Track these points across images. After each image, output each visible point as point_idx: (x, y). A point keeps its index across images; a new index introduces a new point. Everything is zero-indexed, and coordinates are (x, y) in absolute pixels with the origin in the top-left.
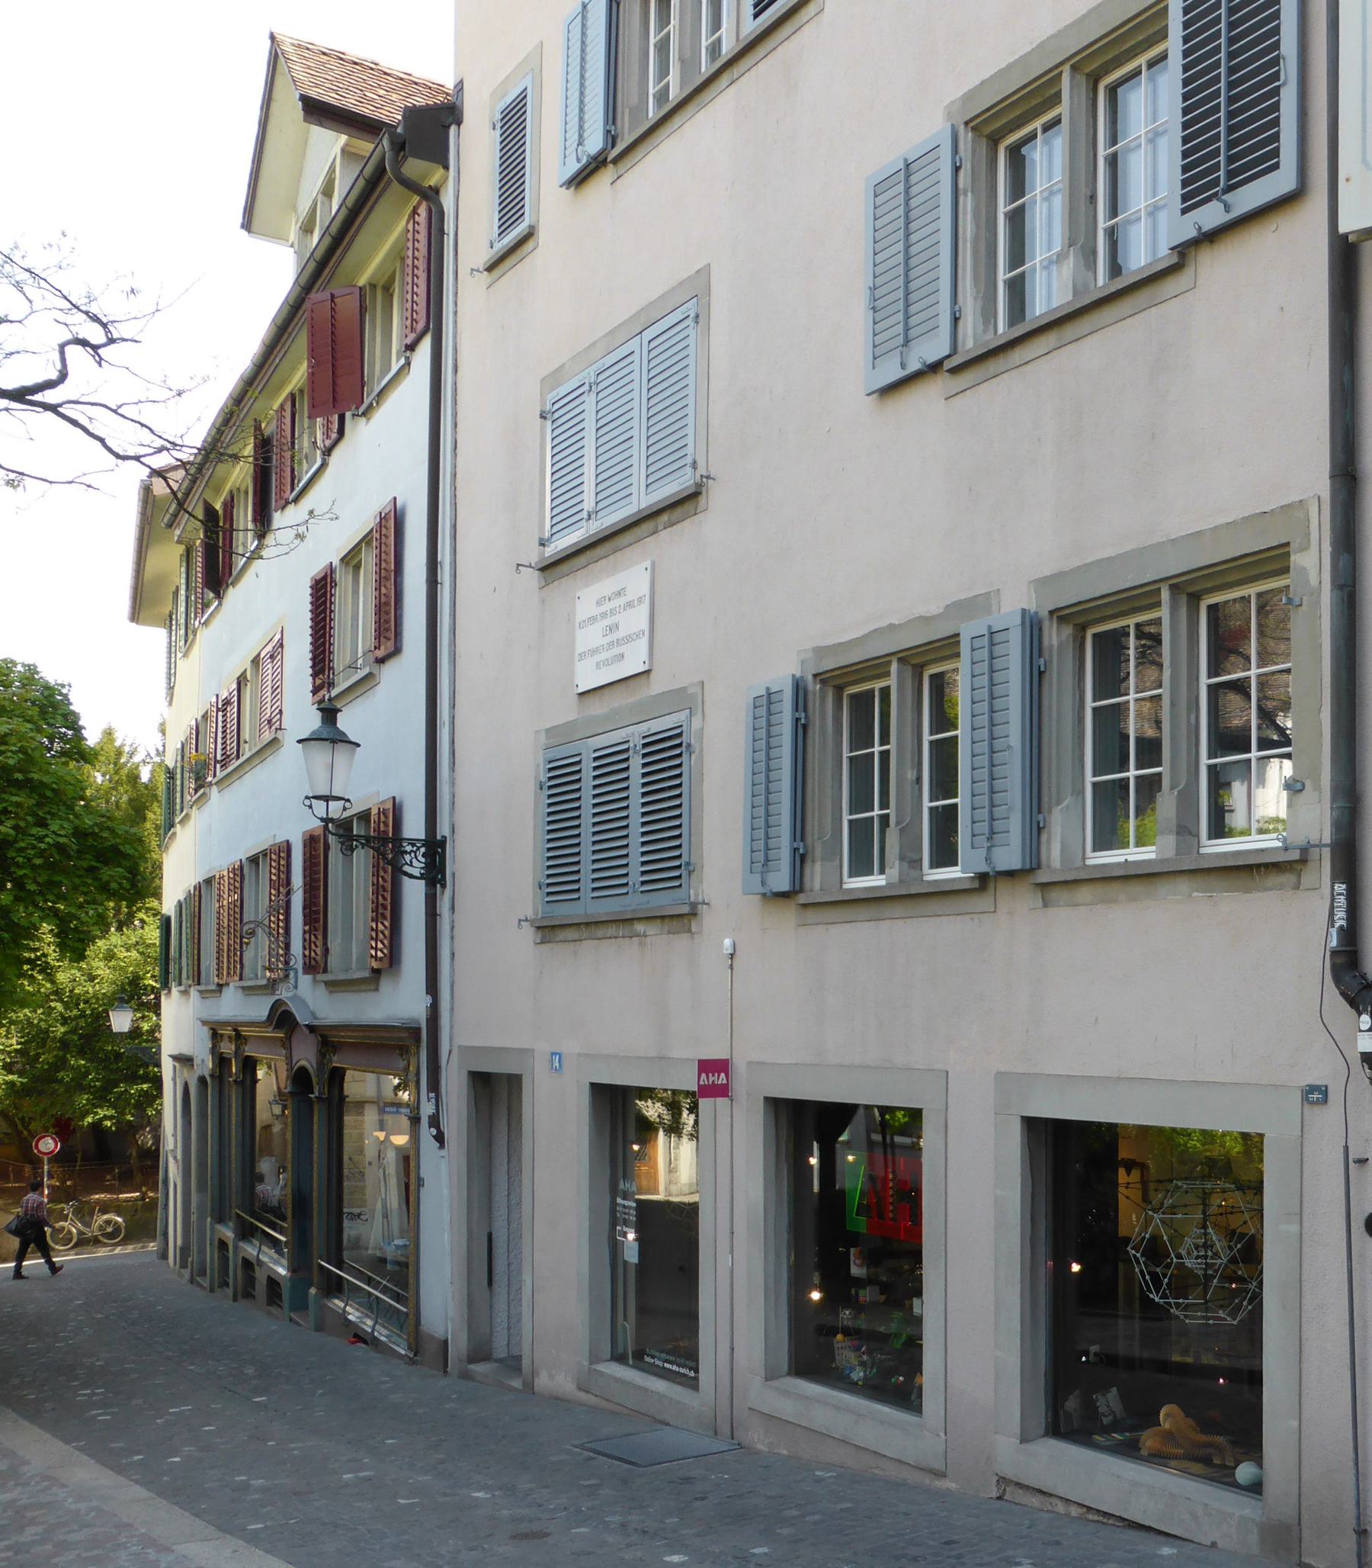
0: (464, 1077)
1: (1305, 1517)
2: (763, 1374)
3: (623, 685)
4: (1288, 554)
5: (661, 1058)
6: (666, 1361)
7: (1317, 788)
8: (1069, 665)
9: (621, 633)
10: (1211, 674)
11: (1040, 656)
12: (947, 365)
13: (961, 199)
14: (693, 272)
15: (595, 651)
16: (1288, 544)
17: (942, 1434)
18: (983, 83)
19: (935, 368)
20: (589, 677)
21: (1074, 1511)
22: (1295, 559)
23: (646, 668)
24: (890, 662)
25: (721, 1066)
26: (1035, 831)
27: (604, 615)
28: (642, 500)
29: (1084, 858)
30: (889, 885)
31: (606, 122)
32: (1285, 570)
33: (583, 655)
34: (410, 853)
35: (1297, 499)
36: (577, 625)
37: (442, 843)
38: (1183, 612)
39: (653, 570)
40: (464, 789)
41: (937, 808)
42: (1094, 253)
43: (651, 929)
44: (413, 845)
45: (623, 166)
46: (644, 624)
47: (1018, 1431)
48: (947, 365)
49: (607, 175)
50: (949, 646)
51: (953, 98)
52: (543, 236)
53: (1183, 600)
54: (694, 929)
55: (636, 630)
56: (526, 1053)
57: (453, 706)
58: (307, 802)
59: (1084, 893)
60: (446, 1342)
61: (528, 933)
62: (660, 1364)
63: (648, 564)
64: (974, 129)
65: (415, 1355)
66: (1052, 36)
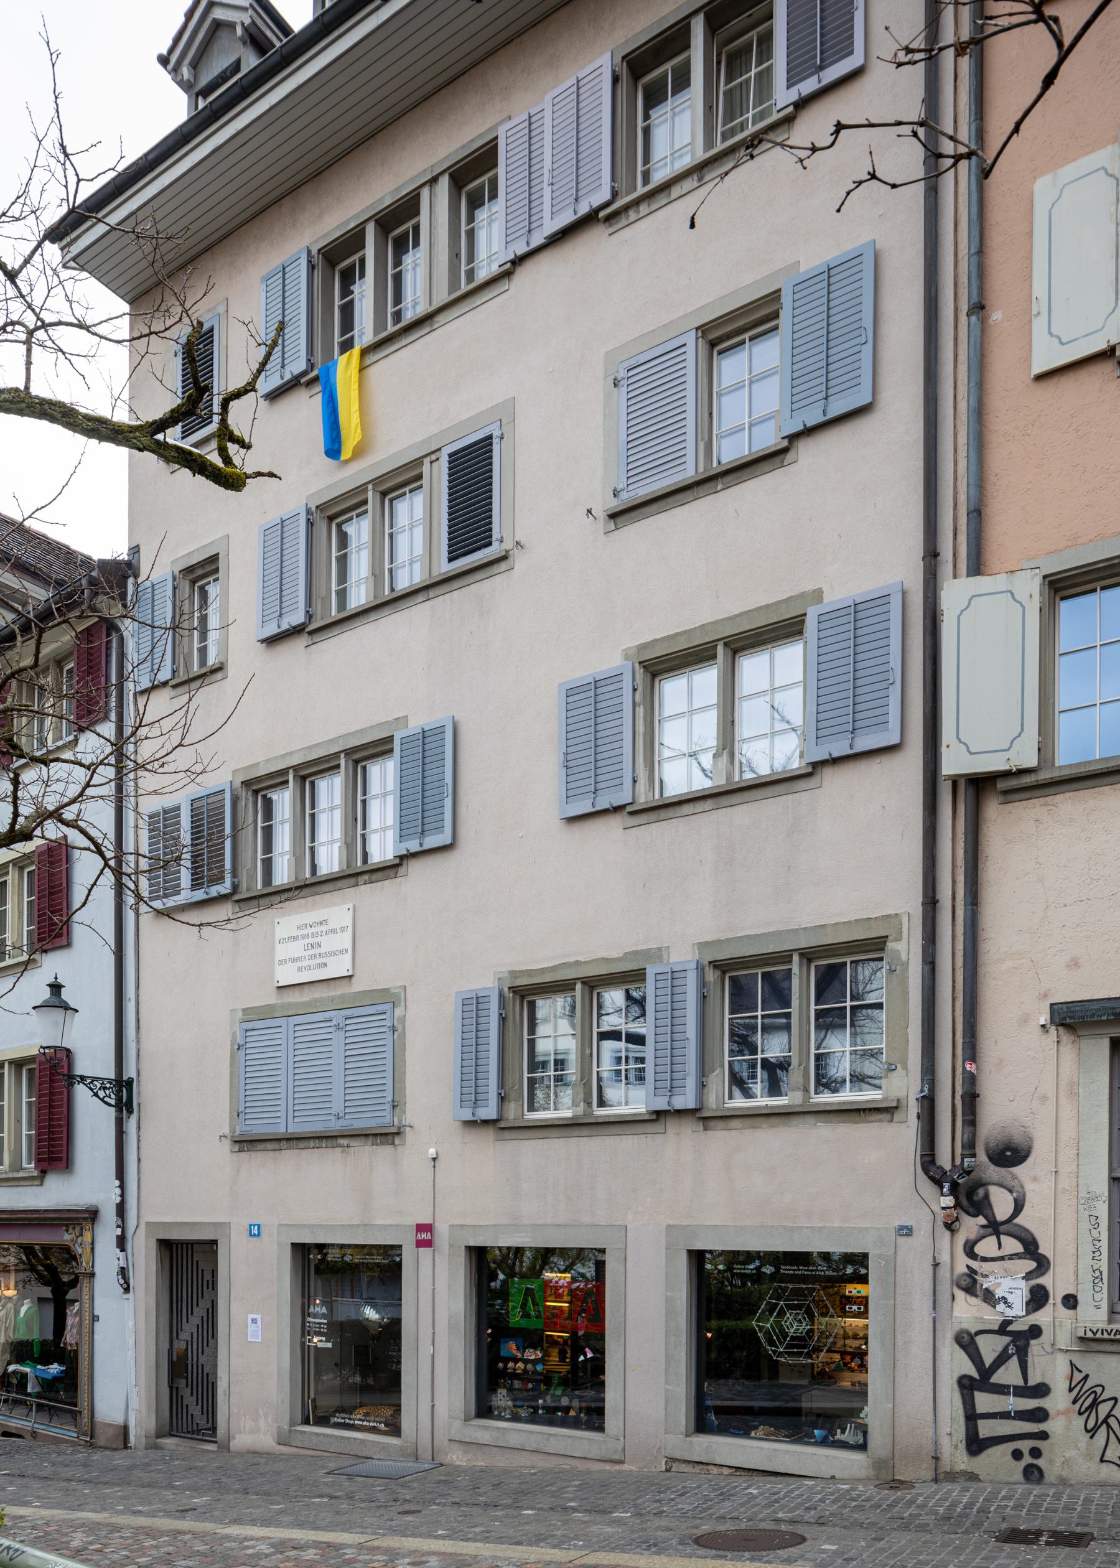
0: (153, 1245)
1: (897, 1456)
2: (463, 1417)
3: (324, 984)
4: (885, 942)
5: (365, 1225)
7: (905, 1068)
8: (719, 993)
9: (323, 950)
10: (817, 1003)
12: (629, 809)
13: (637, 708)
14: (391, 718)
15: (294, 960)
16: (887, 937)
17: (622, 1439)
18: (655, 641)
19: (618, 809)
20: (287, 975)
21: (726, 1471)
22: (890, 945)
23: (350, 973)
24: (575, 984)
26: (702, 1086)
29: (523, 1115)
30: (884, 1099)
31: (306, 607)
32: (883, 949)
33: (281, 962)
34: (109, 1089)
35: (894, 913)
36: (277, 942)
37: (129, 1083)
38: (805, 968)
39: (354, 911)
40: (147, 1045)
43: (354, 1143)
44: (111, 1083)
45: (317, 638)
46: (348, 945)
47: (684, 1431)
49: (302, 641)
51: (629, 646)
53: (805, 961)
55: (339, 949)
56: (225, 1226)
57: (138, 987)
59: (735, 1123)
60: (126, 1428)
61: (227, 1144)
63: (351, 906)
64: (644, 667)
65: (91, 1438)
66: (712, 623)
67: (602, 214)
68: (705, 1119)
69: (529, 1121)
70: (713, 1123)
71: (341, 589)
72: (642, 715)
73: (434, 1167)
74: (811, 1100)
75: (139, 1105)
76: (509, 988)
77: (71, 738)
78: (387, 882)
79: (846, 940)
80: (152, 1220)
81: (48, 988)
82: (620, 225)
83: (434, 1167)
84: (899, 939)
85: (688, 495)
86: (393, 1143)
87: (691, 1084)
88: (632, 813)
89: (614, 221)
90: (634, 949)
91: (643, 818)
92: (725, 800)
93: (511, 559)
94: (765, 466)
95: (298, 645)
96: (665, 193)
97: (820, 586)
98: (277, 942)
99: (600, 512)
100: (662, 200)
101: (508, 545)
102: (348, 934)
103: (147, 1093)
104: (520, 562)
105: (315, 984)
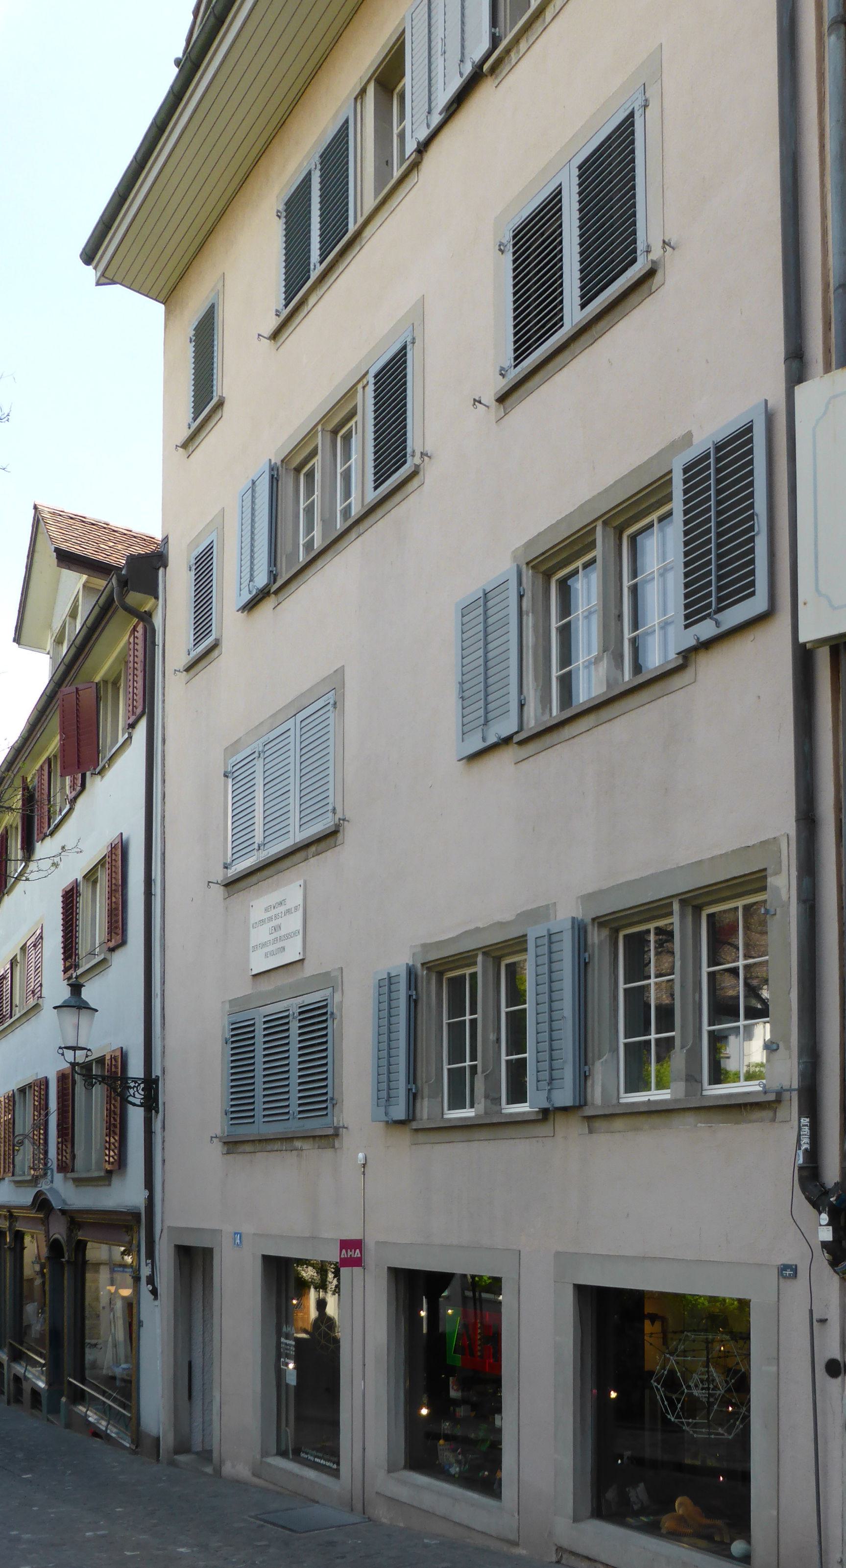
4: (765, 877)
6: (316, 1457)
7: (788, 1048)
9: (283, 932)
11: (585, 951)
12: (516, 739)
13: (525, 617)
14: (332, 671)
15: (264, 945)
16: (765, 870)
17: (516, 1515)
18: (539, 534)
19: (506, 741)
20: (259, 964)
22: (771, 880)
23: (301, 957)
25: (357, 1244)
26: (583, 1078)
27: (270, 919)
28: (297, 836)
29: (618, 1098)
32: (764, 889)
33: (255, 948)
36: (251, 926)
37: (156, 1081)
38: (689, 919)
41: (512, 1060)
42: (622, 656)
43: (306, 1145)
44: (136, 1082)
46: (299, 926)
48: (516, 739)
49: (270, 602)
50: (519, 944)
51: (517, 546)
52: (225, 645)
54: (337, 1145)
57: (163, 983)
58: (61, 1051)
59: (619, 1124)
61: (217, 1148)
62: (312, 1458)
63: (301, 882)
66: (589, 501)
67: (486, 67)
68: (590, 1119)
69: (450, 1120)
70: (597, 1124)
71: (345, 470)
72: (530, 625)
73: (364, 1173)
74: (705, 1093)
75: (164, 1104)
76: (423, 964)
77: (126, 736)
78: (329, 853)
79: (722, 879)
80: (172, 1225)
81: (69, 988)
82: (504, 74)
83: (364, 1173)
84: (778, 872)
85: (566, 355)
86: (333, 1147)
87: (568, 1074)
88: (521, 743)
89: (498, 71)
90: (525, 909)
91: (531, 748)
92: (605, 714)
93: (421, 473)
94: (633, 299)
95: (268, 604)
96: (541, 19)
97: (689, 429)
98: (251, 926)
99: (489, 397)
100: (538, 27)
101: (417, 460)
102: (299, 914)
103: (168, 1093)
104: (431, 474)
105: (272, 974)
